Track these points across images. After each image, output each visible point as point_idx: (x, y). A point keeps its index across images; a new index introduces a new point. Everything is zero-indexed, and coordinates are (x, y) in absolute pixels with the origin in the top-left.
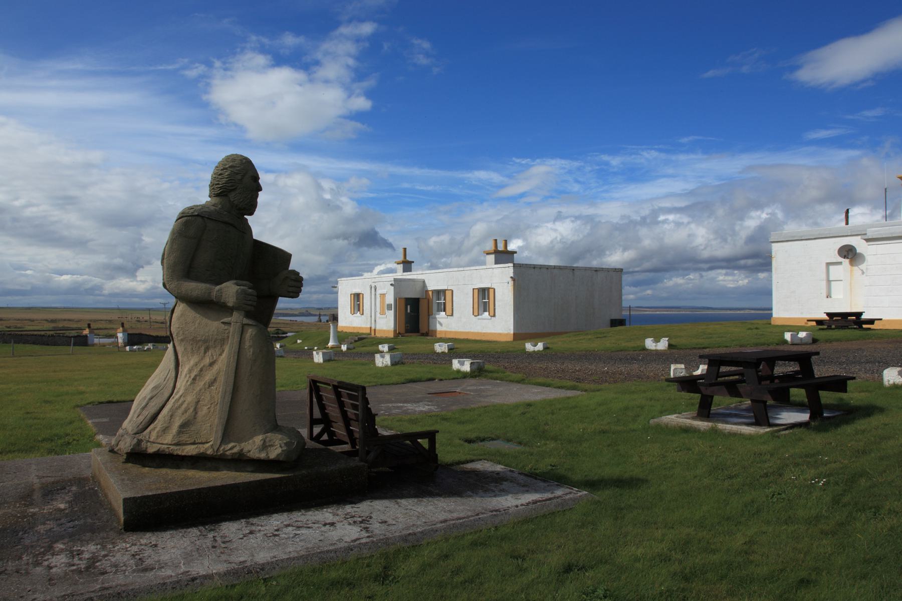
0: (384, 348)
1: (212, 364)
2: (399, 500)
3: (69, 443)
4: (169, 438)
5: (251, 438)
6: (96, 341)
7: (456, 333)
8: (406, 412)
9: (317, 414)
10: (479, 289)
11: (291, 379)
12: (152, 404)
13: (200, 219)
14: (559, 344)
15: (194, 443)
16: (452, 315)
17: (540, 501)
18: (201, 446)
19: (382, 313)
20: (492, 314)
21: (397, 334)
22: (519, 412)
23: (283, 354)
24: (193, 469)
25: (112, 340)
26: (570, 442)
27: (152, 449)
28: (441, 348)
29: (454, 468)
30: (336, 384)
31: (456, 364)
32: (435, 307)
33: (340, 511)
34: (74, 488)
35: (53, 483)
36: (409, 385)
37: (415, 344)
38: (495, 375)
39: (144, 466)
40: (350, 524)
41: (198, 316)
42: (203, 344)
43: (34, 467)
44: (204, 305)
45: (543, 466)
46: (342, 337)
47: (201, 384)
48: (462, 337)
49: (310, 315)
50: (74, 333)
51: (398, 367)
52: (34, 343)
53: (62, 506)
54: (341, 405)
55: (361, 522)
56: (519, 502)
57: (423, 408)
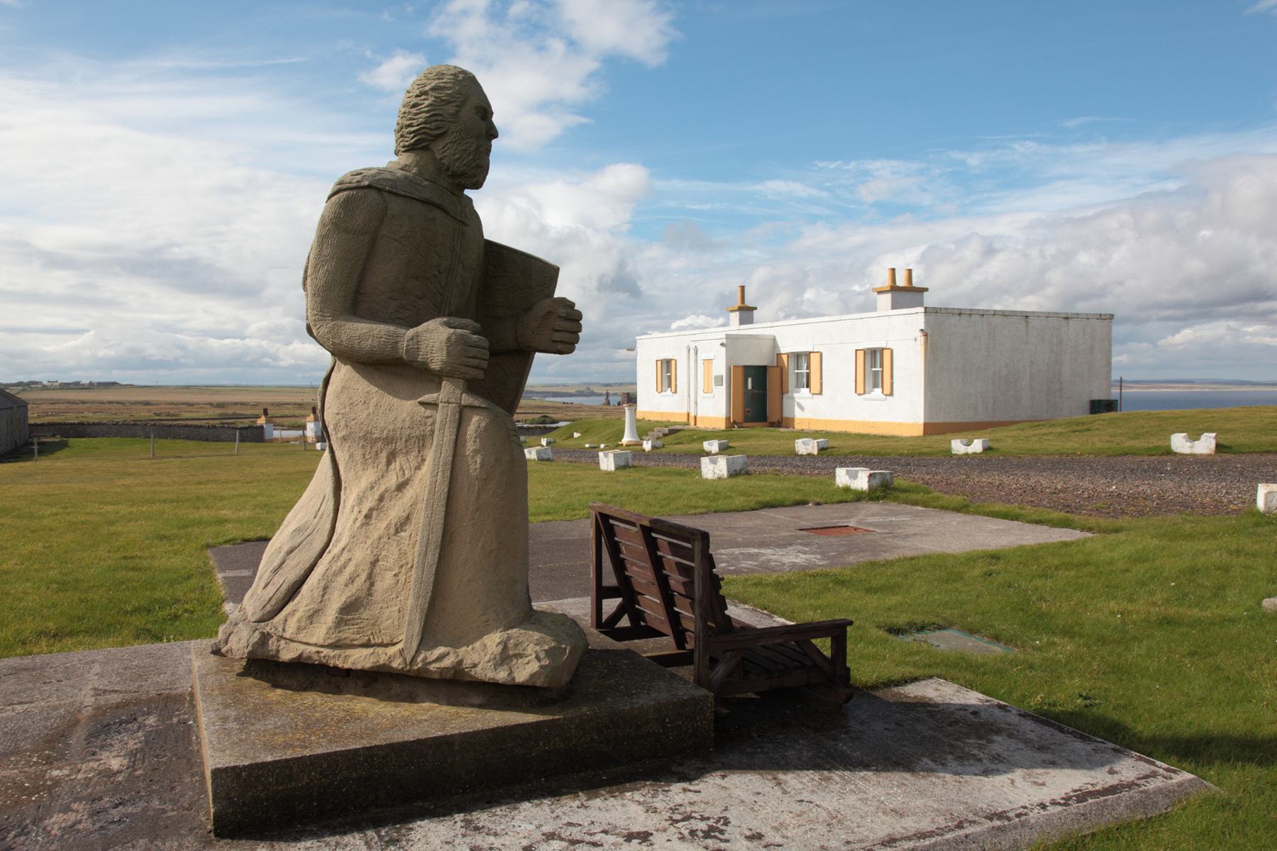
0: (712, 446)
1: (401, 487)
2: (781, 776)
3: (176, 617)
4: (320, 633)
5: (480, 636)
6: (276, 434)
7: (827, 422)
8: (766, 566)
9: (610, 580)
10: (865, 351)
11: (559, 497)
12: (291, 562)
13: (373, 193)
14: (1008, 440)
15: (367, 645)
16: (821, 393)
17: (1093, 794)
18: (380, 650)
19: (707, 390)
20: (887, 391)
21: (731, 424)
22: (977, 572)
23: (551, 456)
24: (366, 695)
25: (300, 432)
26: (1103, 640)
27: (287, 654)
28: (805, 447)
29: (879, 693)
30: (646, 523)
31: (842, 477)
32: (792, 380)
33: (660, 802)
34: (152, 720)
35: (118, 706)
36: (763, 512)
37: (762, 439)
38: (914, 497)
39: (276, 685)
40: (682, 838)
41: (374, 389)
42: (387, 447)
43: (97, 668)
44: (388, 368)
45: (1068, 694)
46: (643, 429)
47: (380, 526)
48: (836, 429)
49: (593, 394)
50: (246, 423)
51: (740, 480)
52: (188, 438)
53: (115, 764)
54: (658, 564)
55: (707, 835)
56: (1046, 794)
57: (794, 557)
